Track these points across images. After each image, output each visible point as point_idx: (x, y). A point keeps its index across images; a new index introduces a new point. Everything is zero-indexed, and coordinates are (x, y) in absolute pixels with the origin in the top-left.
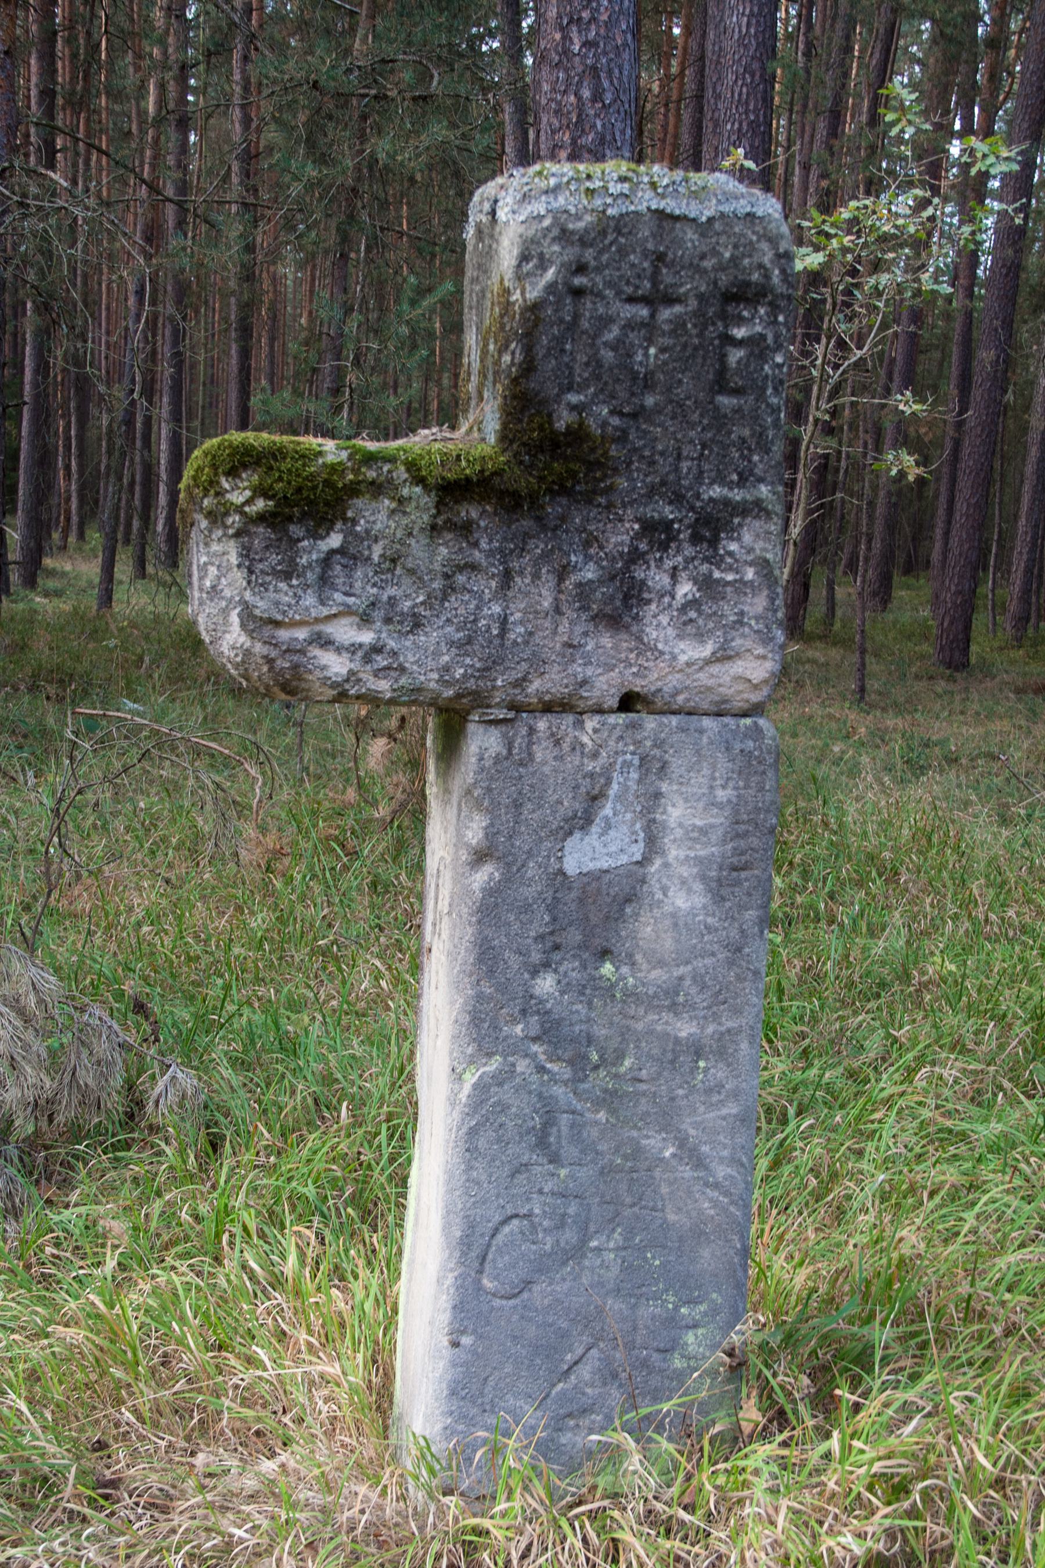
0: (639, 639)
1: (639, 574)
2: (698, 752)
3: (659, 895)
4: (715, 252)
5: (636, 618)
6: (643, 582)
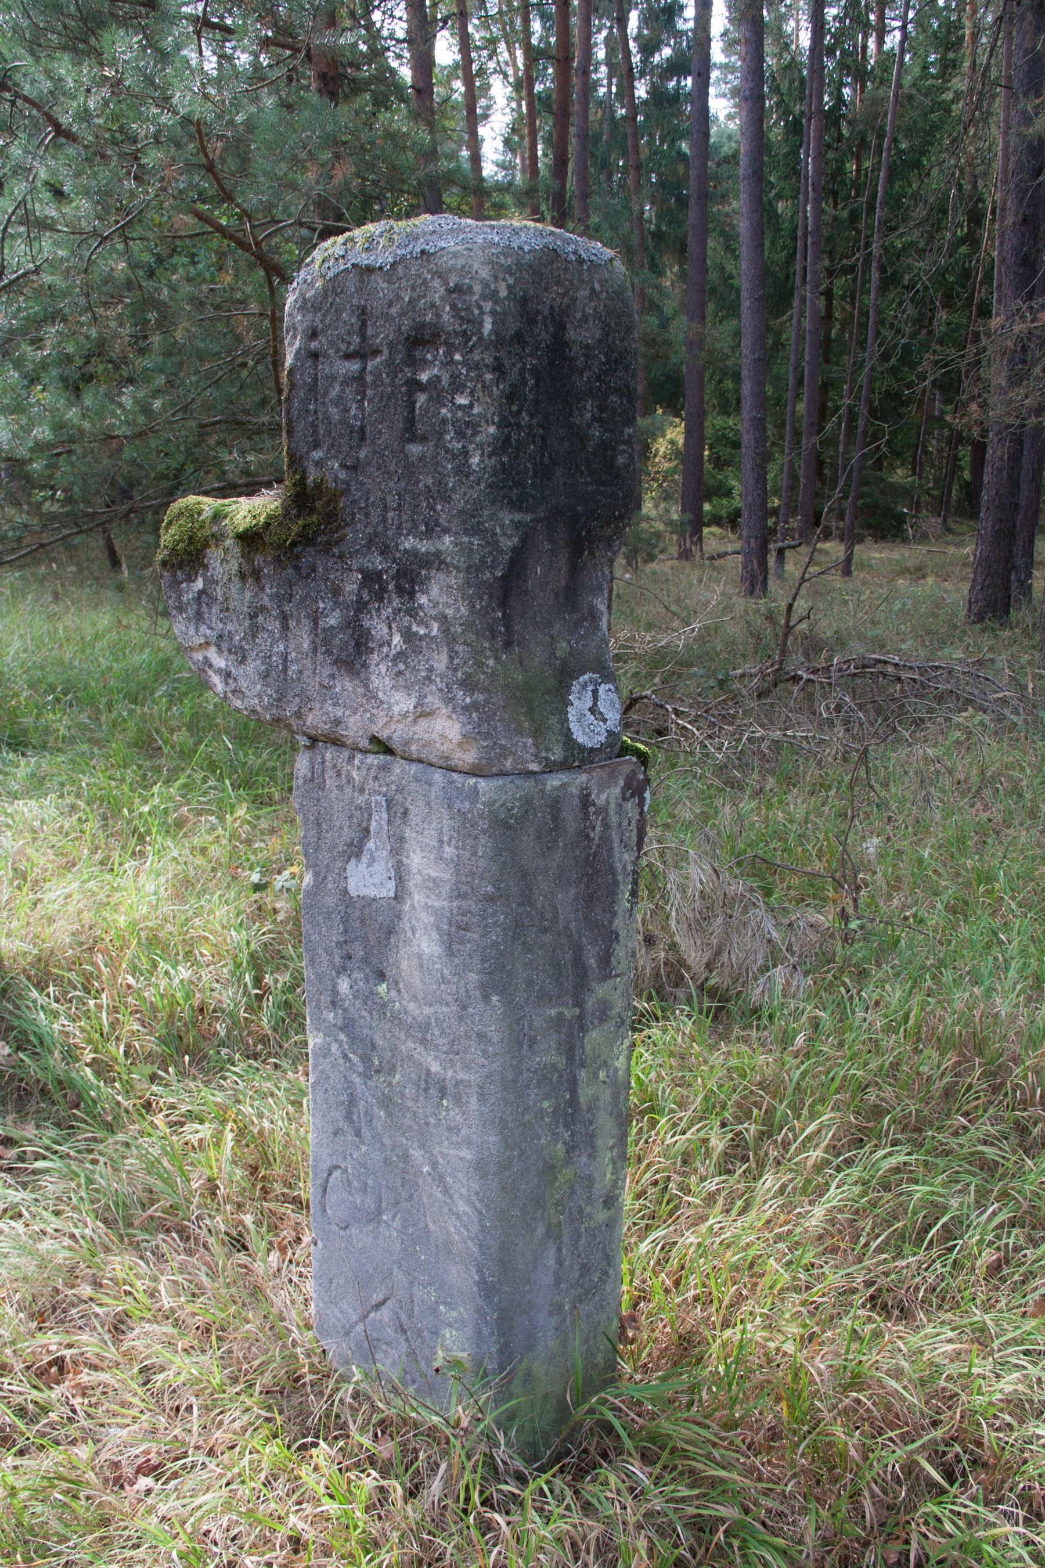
0: (366, 686)
1: (366, 623)
2: (428, 804)
3: (409, 934)
4: (399, 298)
5: (365, 666)
6: (369, 630)
